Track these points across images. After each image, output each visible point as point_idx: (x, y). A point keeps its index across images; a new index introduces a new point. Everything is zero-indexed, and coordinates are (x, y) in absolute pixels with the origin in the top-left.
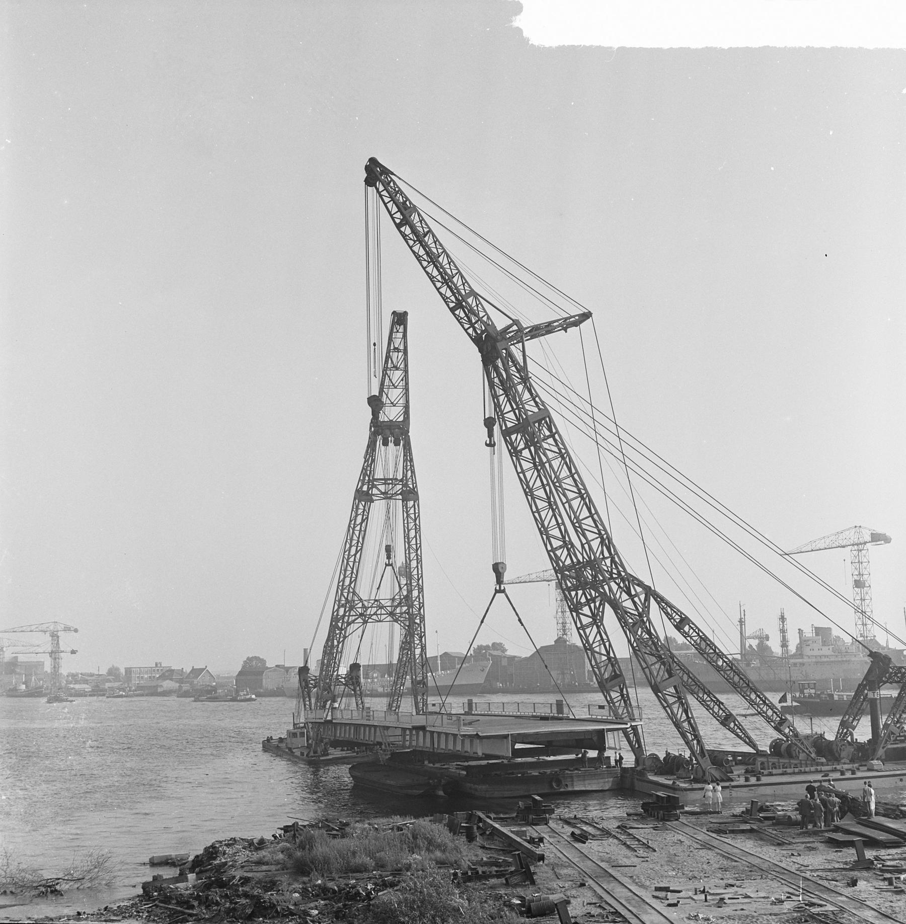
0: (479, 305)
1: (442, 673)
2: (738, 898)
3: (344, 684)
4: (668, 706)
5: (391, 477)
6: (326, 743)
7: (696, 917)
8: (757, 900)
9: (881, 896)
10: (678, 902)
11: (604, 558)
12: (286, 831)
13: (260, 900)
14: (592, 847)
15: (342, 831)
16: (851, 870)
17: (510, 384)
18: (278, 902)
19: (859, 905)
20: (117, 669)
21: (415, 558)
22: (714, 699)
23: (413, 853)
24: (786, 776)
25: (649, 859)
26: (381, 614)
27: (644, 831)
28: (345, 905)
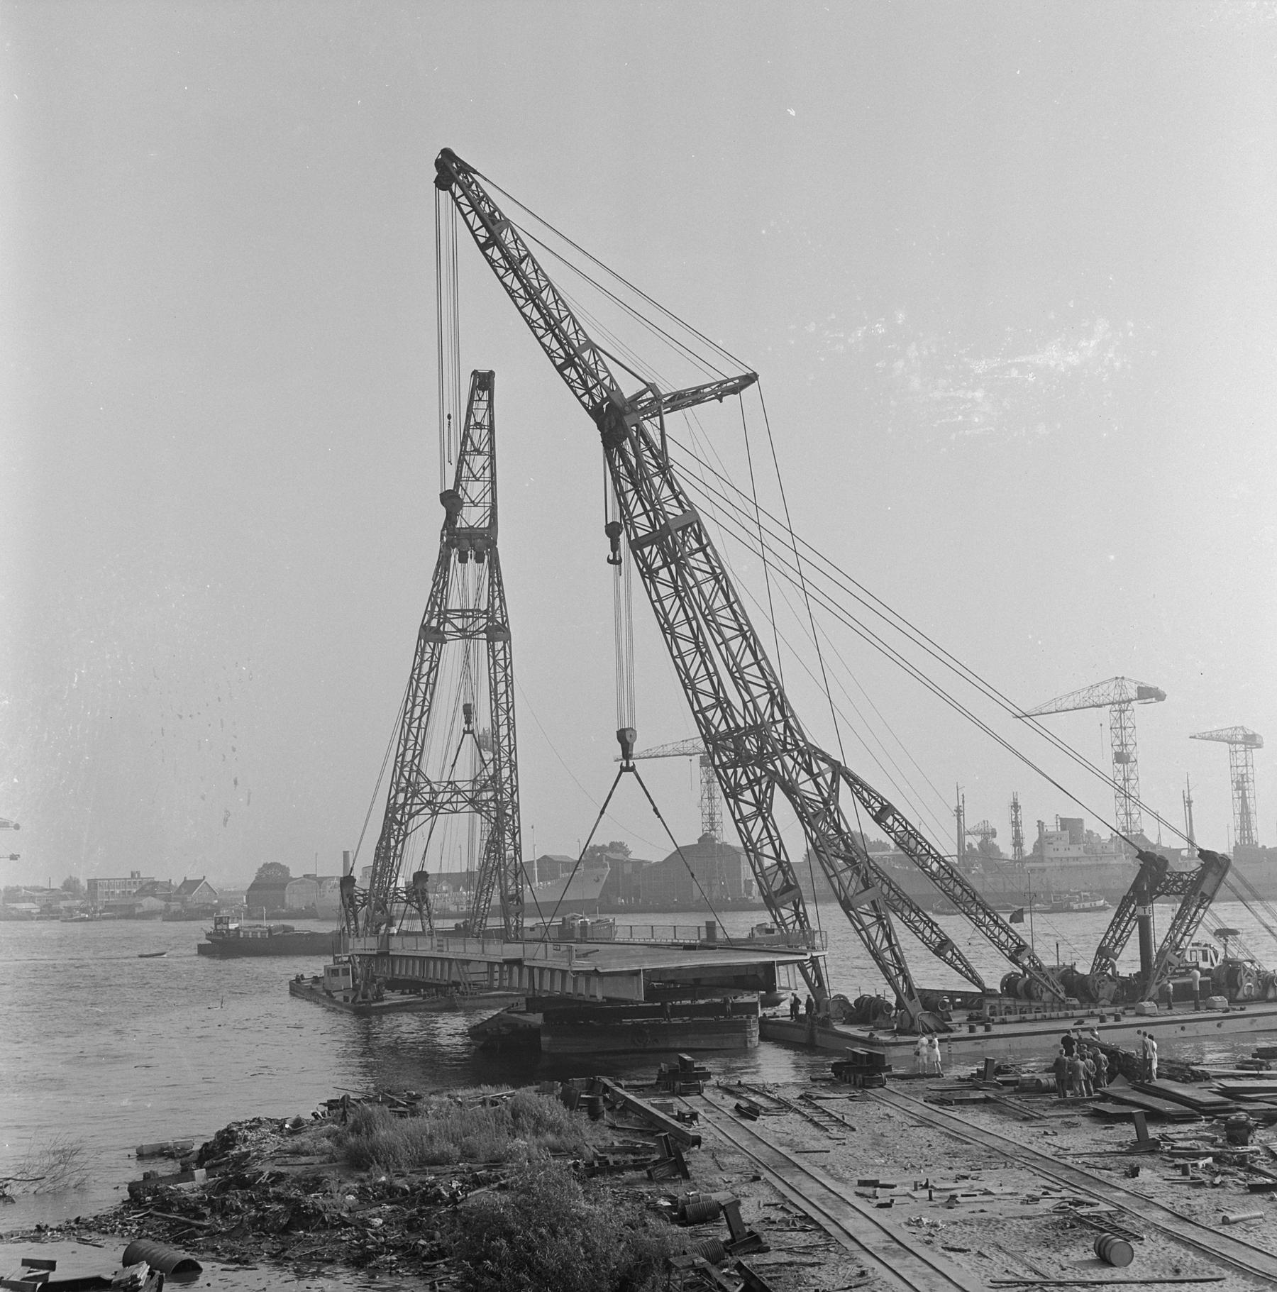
0: (599, 362)
1: (540, 885)
2: (975, 1195)
3: (406, 901)
4: (863, 929)
5: (471, 607)
6: (380, 985)
7: (918, 1223)
8: (1002, 1197)
9: (1173, 1190)
10: (892, 1201)
11: (775, 722)
12: (330, 1108)
13: (299, 1205)
14: (763, 1125)
15: (412, 1107)
16: (1128, 1153)
17: (641, 474)
18: (325, 1208)
19: (1145, 1203)
20: (77, 881)
21: (506, 722)
22: (925, 919)
23: (515, 1137)
24: (1023, 1024)
25: (846, 1142)
26: (457, 802)
27: (837, 1103)
28: (420, 1212)
